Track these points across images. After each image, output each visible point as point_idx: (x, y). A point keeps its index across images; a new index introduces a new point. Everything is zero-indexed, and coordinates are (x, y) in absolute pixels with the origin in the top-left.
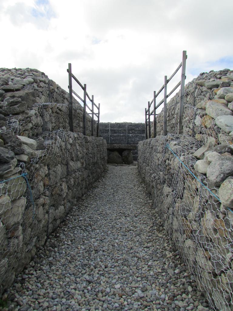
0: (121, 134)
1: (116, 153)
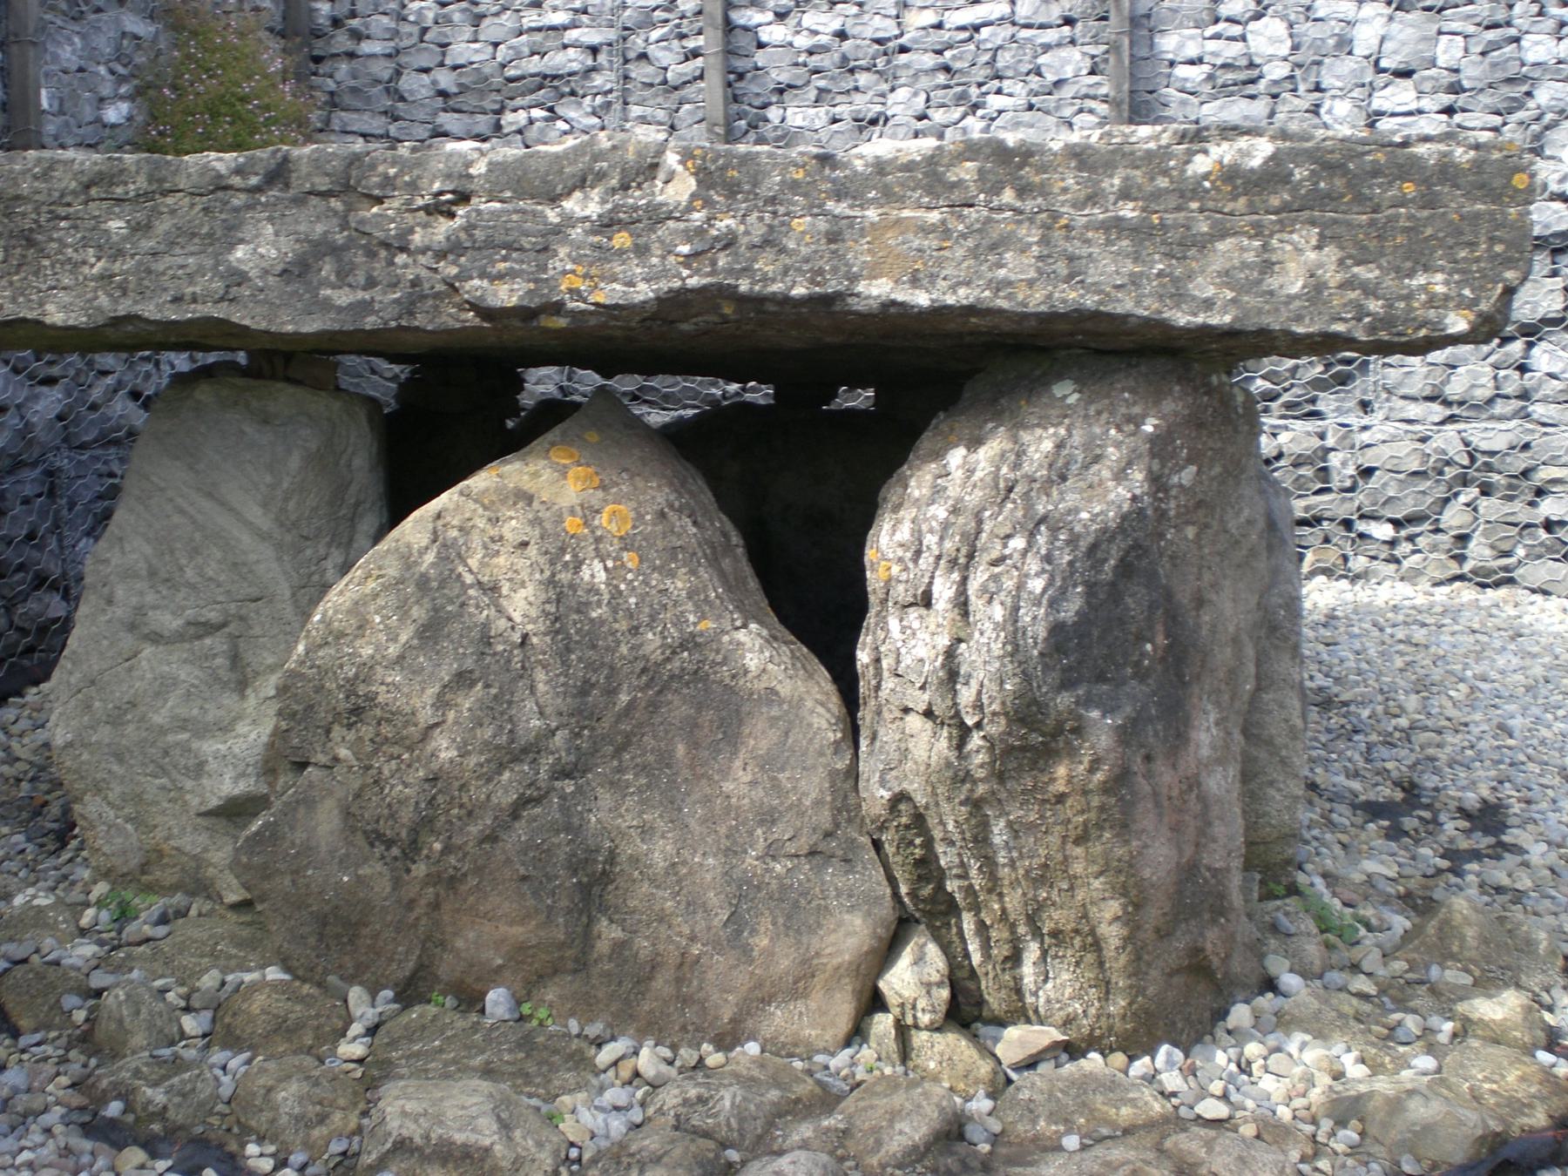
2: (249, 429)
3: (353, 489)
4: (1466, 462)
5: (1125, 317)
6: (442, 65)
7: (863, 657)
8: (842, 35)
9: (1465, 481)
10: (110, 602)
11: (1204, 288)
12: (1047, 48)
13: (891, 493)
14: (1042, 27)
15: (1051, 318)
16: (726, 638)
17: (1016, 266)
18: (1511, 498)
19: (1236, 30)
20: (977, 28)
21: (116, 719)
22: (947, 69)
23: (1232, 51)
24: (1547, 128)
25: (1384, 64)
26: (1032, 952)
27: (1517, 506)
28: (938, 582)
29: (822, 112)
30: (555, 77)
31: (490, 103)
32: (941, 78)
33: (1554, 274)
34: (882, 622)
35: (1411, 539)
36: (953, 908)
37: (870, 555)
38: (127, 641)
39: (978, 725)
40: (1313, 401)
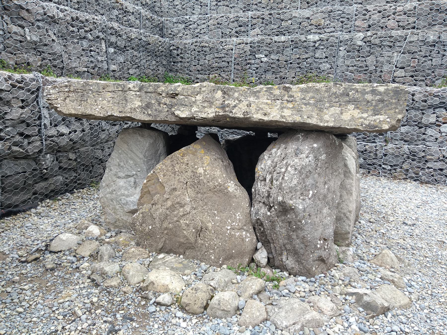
0: (311, 37)
1: (206, 165)
2: (139, 138)
3: (159, 151)
4: (409, 154)
5: (309, 124)
6: (198, 64)
7: (253, 190)
8: (278, 60)
9: (408, 158)
10: (111, 170)
11: (326, 117)
12: (321, 63)
13: (261, 157)
14: (321, 58)
15: (294, 123)
16: (226, 185)
17: (287, 113)
18: (419, 162)
19: (363, 59)
20: (307, 59)
21: (111, 193)
22: (300, 67)
23: (363, 64)
24: (437, 80)
25: (397, 66)
26: (285, 253)
27: (421, 164)
28: (267, 176)
29: (274, 76)
30: (220, 68)
31: (208, 72)
32: (298, 70)
33: (434, 113)
34: (257, 182)
35: (395, 169)
36: (269, 242)
37: (256, 170)
38: (115, 179)
39: (273, 206)
40: (374, 139)
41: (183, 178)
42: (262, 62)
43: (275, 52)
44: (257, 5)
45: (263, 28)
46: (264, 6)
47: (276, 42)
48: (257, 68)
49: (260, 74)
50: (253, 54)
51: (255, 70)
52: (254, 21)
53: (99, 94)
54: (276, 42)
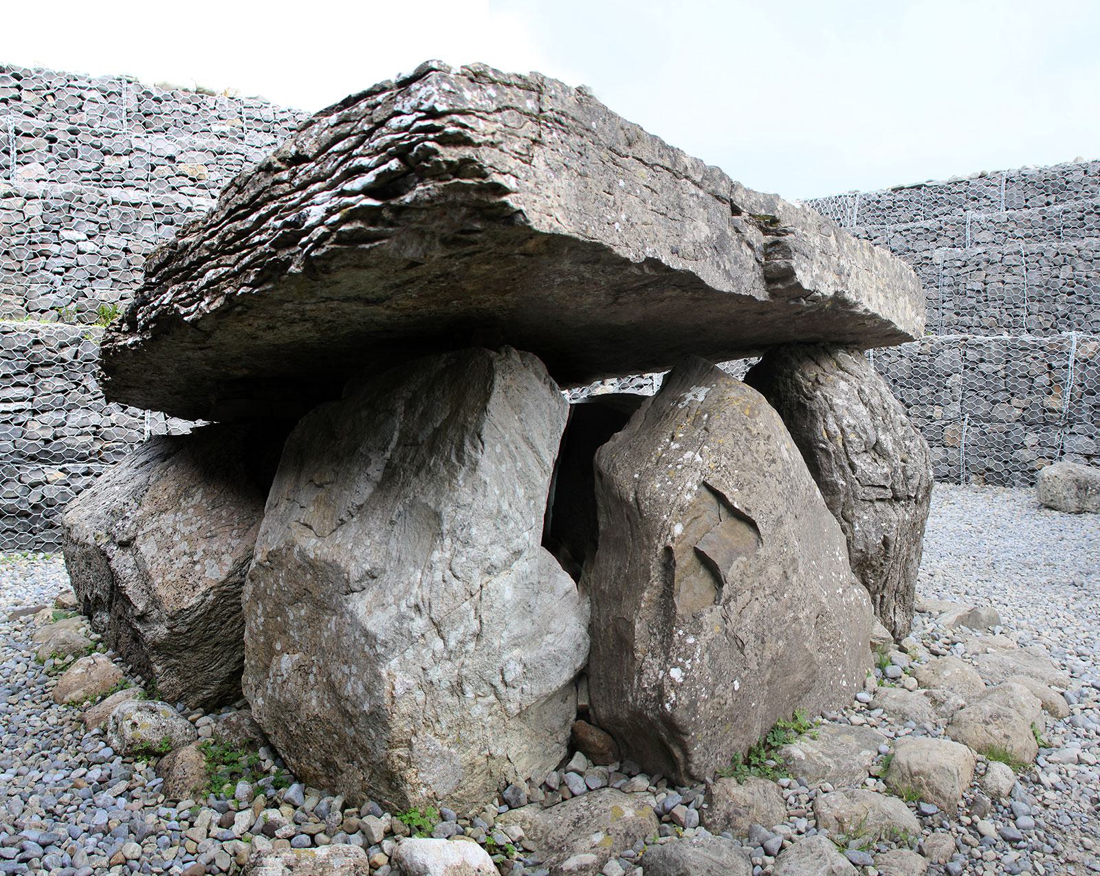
8: (126, 250)
41: (743, 438)
42: (80, 252)
43: (118, 228)
44: (7, 103)
45: (52, 165)
46: (30, 110)
47: (114, 203)
48: (67, 269)
49: (79, 285)
50: (53, 228)
51: (61, 274)
52: (27, 143)
53: (618, 160)
54: (114, 203)
